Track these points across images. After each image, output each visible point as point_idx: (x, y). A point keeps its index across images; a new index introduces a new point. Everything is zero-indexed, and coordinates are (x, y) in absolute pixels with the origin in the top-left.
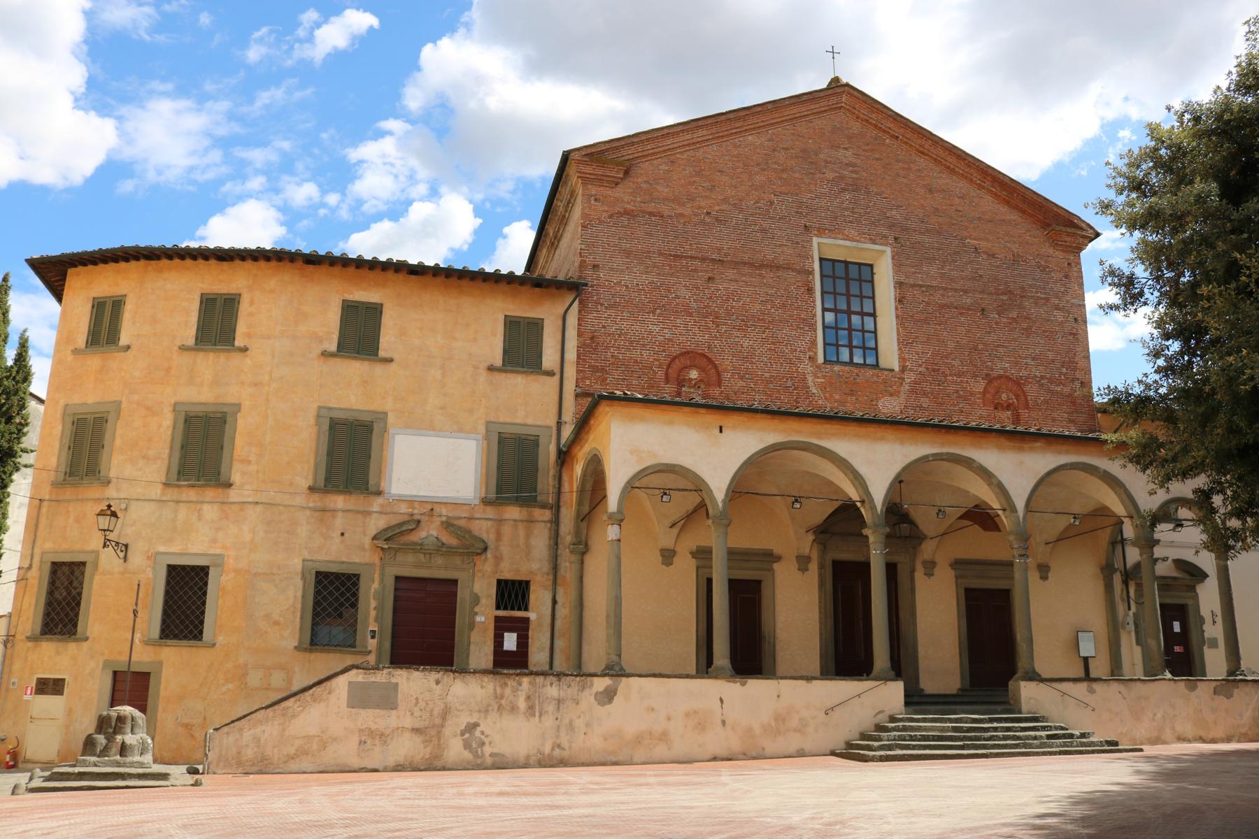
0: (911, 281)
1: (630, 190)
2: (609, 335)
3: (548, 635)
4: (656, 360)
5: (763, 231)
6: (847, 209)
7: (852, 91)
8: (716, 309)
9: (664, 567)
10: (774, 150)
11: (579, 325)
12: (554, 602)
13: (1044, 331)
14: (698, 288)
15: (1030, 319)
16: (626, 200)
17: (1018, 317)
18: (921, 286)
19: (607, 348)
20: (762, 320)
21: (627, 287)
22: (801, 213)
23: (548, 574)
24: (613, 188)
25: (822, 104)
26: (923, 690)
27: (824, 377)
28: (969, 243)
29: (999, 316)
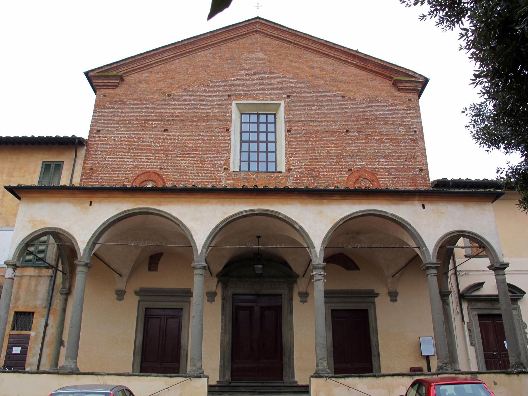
0: (297, 119)
1: (124, 89)
2: (101, 166)
3: (40, 346)
4: (127, 178)
5: (202, 101)
6: (256, 83)
7: (261, 21)
8: (167, 147)
9: (118, 301)
10: (213, 58)
11: (84, 163)
12: (47, 325)
13: (391, 140)
14: (156, 136)
15: (381, 134)
16: (121, 94)
17: (372, 133)
18: (303, 121)
19: (98, 174)
20: (195, 150)
21: (115, 140)
22: (227, 89)
23: (45, 308)
24: (114, 89)
25: (243, 30)
26: (297, 382)
27: (233, 180)
28: (338, 94)
29: (359, 133)
